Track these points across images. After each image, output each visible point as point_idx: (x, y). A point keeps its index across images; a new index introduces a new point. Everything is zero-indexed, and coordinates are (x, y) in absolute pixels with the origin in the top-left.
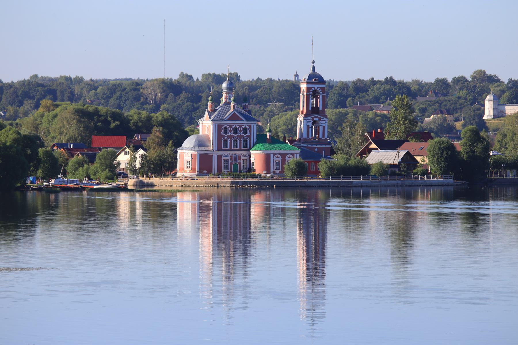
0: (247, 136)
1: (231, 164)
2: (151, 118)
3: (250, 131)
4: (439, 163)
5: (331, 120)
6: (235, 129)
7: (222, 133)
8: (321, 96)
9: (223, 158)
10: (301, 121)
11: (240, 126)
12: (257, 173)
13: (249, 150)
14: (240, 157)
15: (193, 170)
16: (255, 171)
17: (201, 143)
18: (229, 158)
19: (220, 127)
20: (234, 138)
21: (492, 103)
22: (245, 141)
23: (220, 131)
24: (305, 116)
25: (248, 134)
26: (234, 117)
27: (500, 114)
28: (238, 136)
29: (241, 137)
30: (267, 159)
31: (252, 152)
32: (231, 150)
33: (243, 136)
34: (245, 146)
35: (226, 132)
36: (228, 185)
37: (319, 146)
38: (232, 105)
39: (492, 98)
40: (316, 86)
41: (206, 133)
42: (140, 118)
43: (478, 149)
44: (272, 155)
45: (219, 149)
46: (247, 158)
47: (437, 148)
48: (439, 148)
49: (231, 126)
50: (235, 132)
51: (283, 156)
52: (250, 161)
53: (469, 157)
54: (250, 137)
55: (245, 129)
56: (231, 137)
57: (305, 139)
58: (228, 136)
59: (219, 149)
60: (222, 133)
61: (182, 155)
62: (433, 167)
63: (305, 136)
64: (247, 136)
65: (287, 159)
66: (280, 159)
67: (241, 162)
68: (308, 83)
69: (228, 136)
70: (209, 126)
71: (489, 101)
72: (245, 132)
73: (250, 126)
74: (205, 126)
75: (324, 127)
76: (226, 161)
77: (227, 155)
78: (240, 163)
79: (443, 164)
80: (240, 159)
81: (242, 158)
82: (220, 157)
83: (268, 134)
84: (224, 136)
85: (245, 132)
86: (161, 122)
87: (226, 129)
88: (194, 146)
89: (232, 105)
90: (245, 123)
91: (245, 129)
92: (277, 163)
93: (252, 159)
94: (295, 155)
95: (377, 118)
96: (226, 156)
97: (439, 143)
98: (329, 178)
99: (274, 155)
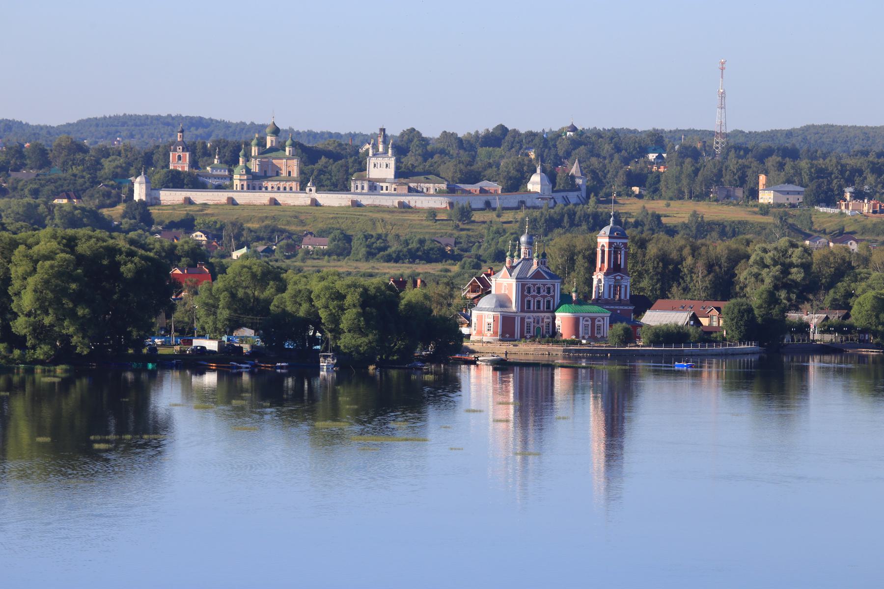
1: (534, 327)
2: (175, 247)
3: (554, 291)
4: (738, 328)
5: (18, 213)
6: (539, 288)
7: (525, 293)
8: (623, 252)
9: (526, 320)
10: (600, 281)
11: (544, 285)
12: (564, 337)
13: (554, 311)
14: (543, 319)
15: (495, 333)
16: (562, 335)
17: (502, 303)
18: (532, 320)
19: (523, 286)
20: (537, 299)
21: (144, 186)
22: (549, 302)
23: (524, 289)
24: (606, 274)
26: (537, 275)
27: (154, 201)
29: (544, 297)
30: (576, 322)
31: (557, 314)
32: (534, 312)
34: (548, 308)
35: (529, 292)
36: (560, 353)
37: (621, 307)
38: (535, 261)
39: (144, 180)
40: (618, 241)
41: (503, 292)
42: (162, 247)
43: (775, 311)
44: (581, 318)
45: (522, 311)
46: (550, 320)
47: (736, 311)
48: (739, 311)
49: (534, 285)
50: (539, 292)
51: (593, 320)
52: (554, 324)
53: (763, 320)
54: (553, 297)
55: (549, 289)
56: (534, 297)
57: (606, 300)
58: (532, 296)
59: (522, 311)
60: (525, 293)
61: (480, 318)
62: (730, 331)
63: (606, 296)
65: (597, 323)
66: (589, 323)
67: (544, 325)
68: (610, 237)
69: (532, 296)
70: (510, 285)
71: (140, 183)
72: (549, 292)
73: (554, 285)
74: (501, 284)
75: (626, 286)
76: (529, 324)
77: (530, 317)
79: (743, 328)
80: (543, 322)
81: (545, 320)
82: (523, 319)
83: (574, 295)
84: (527, 296)
85: (549, 292)
86: (188, 252)
87: (529, 288)
88: (496, 307)
89: (535, 261)
90: (549, 282)
91: (549, 289)
92: (586, 326)
93: (557, 322)
95: (77, 212)
96: (529, 318)
97: (738, 304)
98: (650, 346)
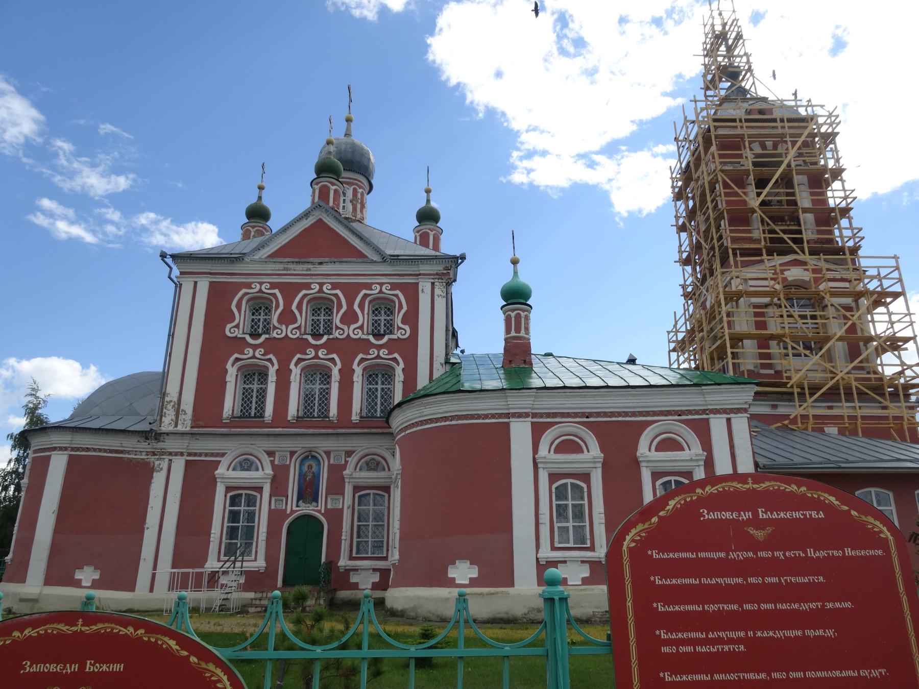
0: (392, 346)
1: (276, 517)
3: (412, 318)
11: (351, 291)
14: (336, 472)
18: (263, 474)
25: (402, 332)
28: (331, 346)
33: (364, 345)
44: (520, 432)
54: (408, 348)
64: (392, 346)
66: (593, 452)
69: (272, 346)
78: (335, 516)
80: (336, 487)
81: (353, 474)
92: (566, 487)
94: (717, 425)
96: (246, 465)
99: (538, 431)
